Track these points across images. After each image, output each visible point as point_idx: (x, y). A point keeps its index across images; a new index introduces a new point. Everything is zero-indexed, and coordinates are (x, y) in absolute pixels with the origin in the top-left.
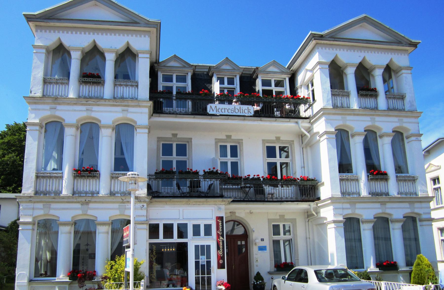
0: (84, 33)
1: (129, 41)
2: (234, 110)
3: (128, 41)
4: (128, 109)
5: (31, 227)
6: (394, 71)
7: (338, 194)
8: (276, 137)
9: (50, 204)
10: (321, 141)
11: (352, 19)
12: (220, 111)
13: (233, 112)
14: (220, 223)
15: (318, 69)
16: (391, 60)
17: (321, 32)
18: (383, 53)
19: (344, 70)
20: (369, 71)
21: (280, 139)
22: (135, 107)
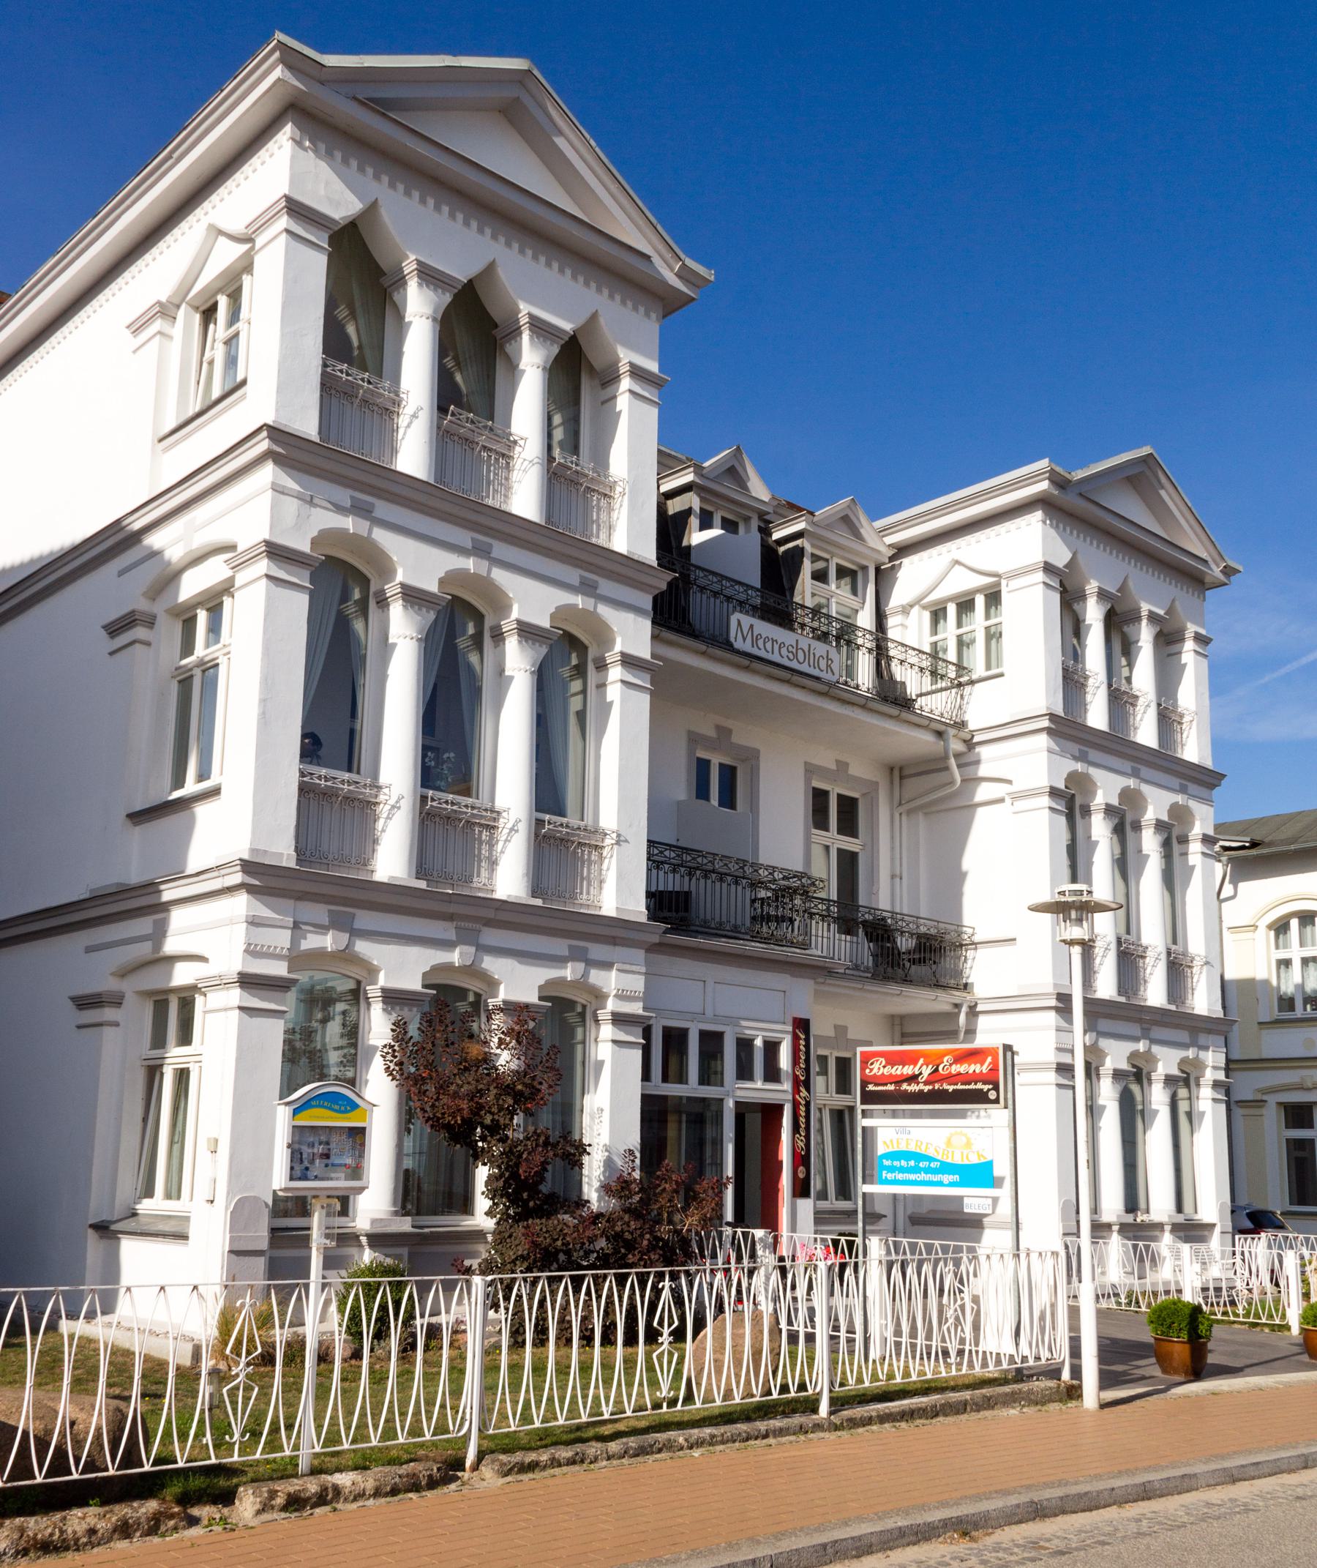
0: (405, 188)
1: (380, 202)
2: (794, 651)
3: (494, 260)
4: (373, 505)
5: (239, 935)
6: (592, 370)
7: (283, 851)
8: (838, 762)
9: (1149, 1029)
10: (237, 585)
11: (1130, 453)
12: (761, 643)
13: (791, 656)
14: (979, 1065)
15: (281, 232)
16: (490, 269)
17: (323, 50)
18: (542, 259)
19: (509, 341)
20: (498, 333)
21: (846, 771)
22: (642, 590)
